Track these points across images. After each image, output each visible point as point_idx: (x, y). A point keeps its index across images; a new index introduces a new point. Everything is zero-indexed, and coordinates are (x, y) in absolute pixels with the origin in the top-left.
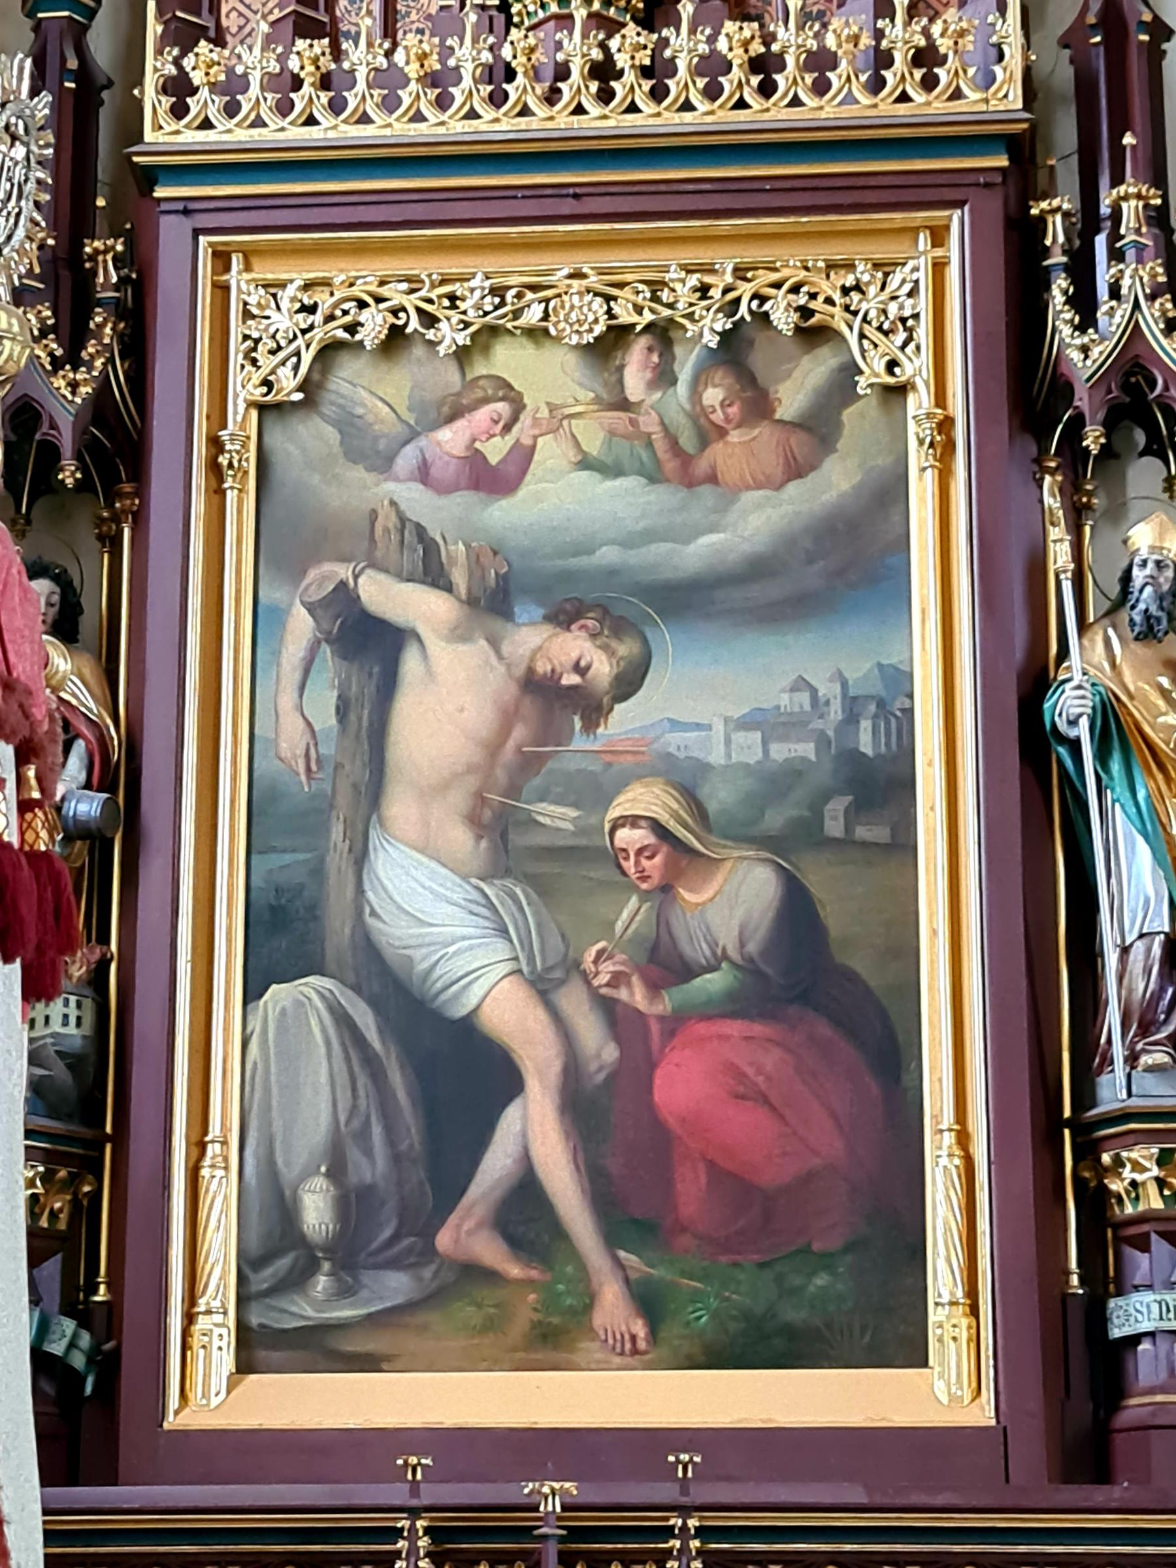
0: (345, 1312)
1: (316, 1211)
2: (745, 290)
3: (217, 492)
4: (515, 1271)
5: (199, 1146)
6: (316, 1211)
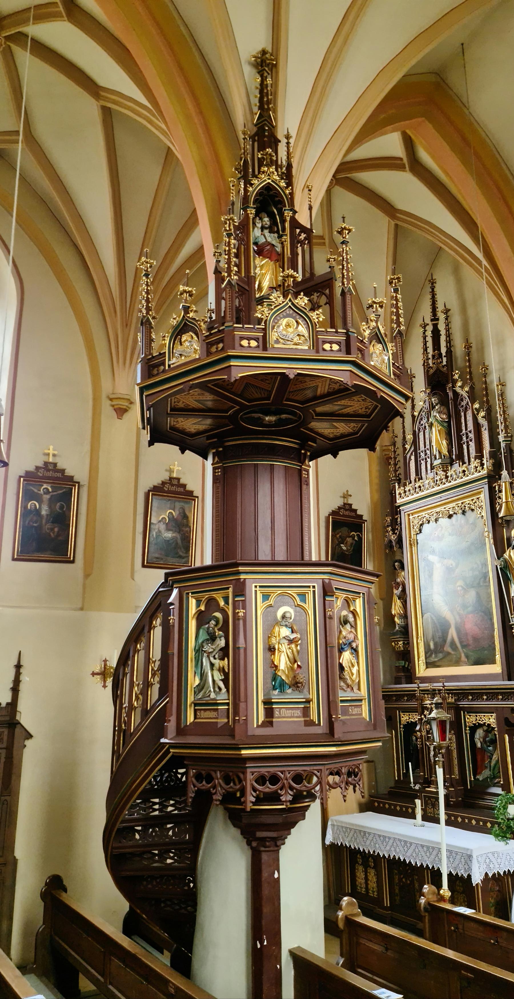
0: (436, 660)
1: (432, 646)
2: (463, 505)
3: (411, 548)
4: (453, 653)
5: (417, 638)
6: (432, 646)
